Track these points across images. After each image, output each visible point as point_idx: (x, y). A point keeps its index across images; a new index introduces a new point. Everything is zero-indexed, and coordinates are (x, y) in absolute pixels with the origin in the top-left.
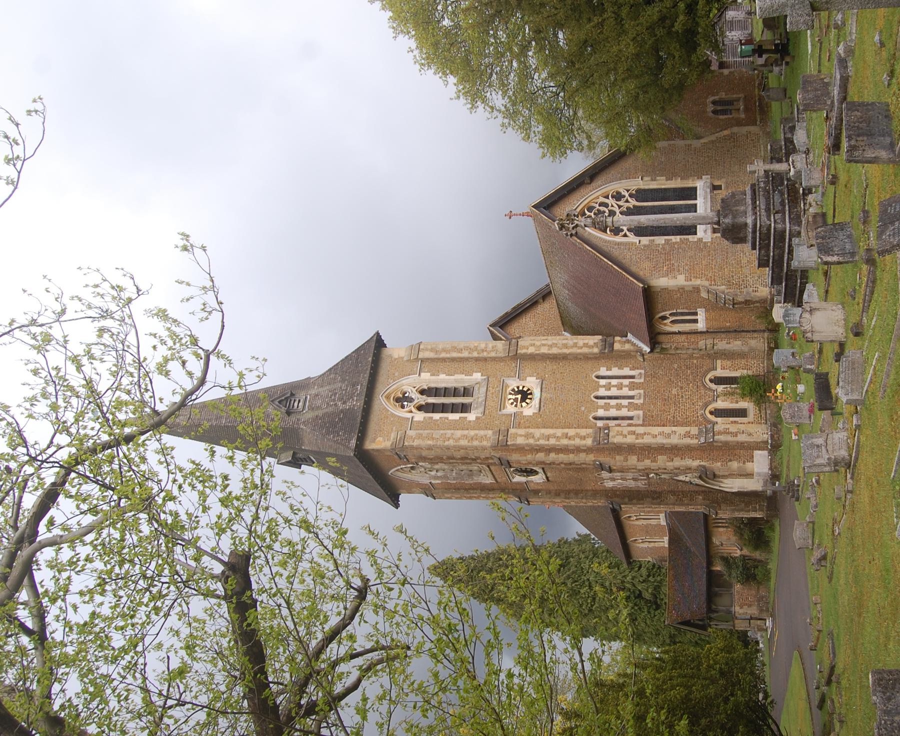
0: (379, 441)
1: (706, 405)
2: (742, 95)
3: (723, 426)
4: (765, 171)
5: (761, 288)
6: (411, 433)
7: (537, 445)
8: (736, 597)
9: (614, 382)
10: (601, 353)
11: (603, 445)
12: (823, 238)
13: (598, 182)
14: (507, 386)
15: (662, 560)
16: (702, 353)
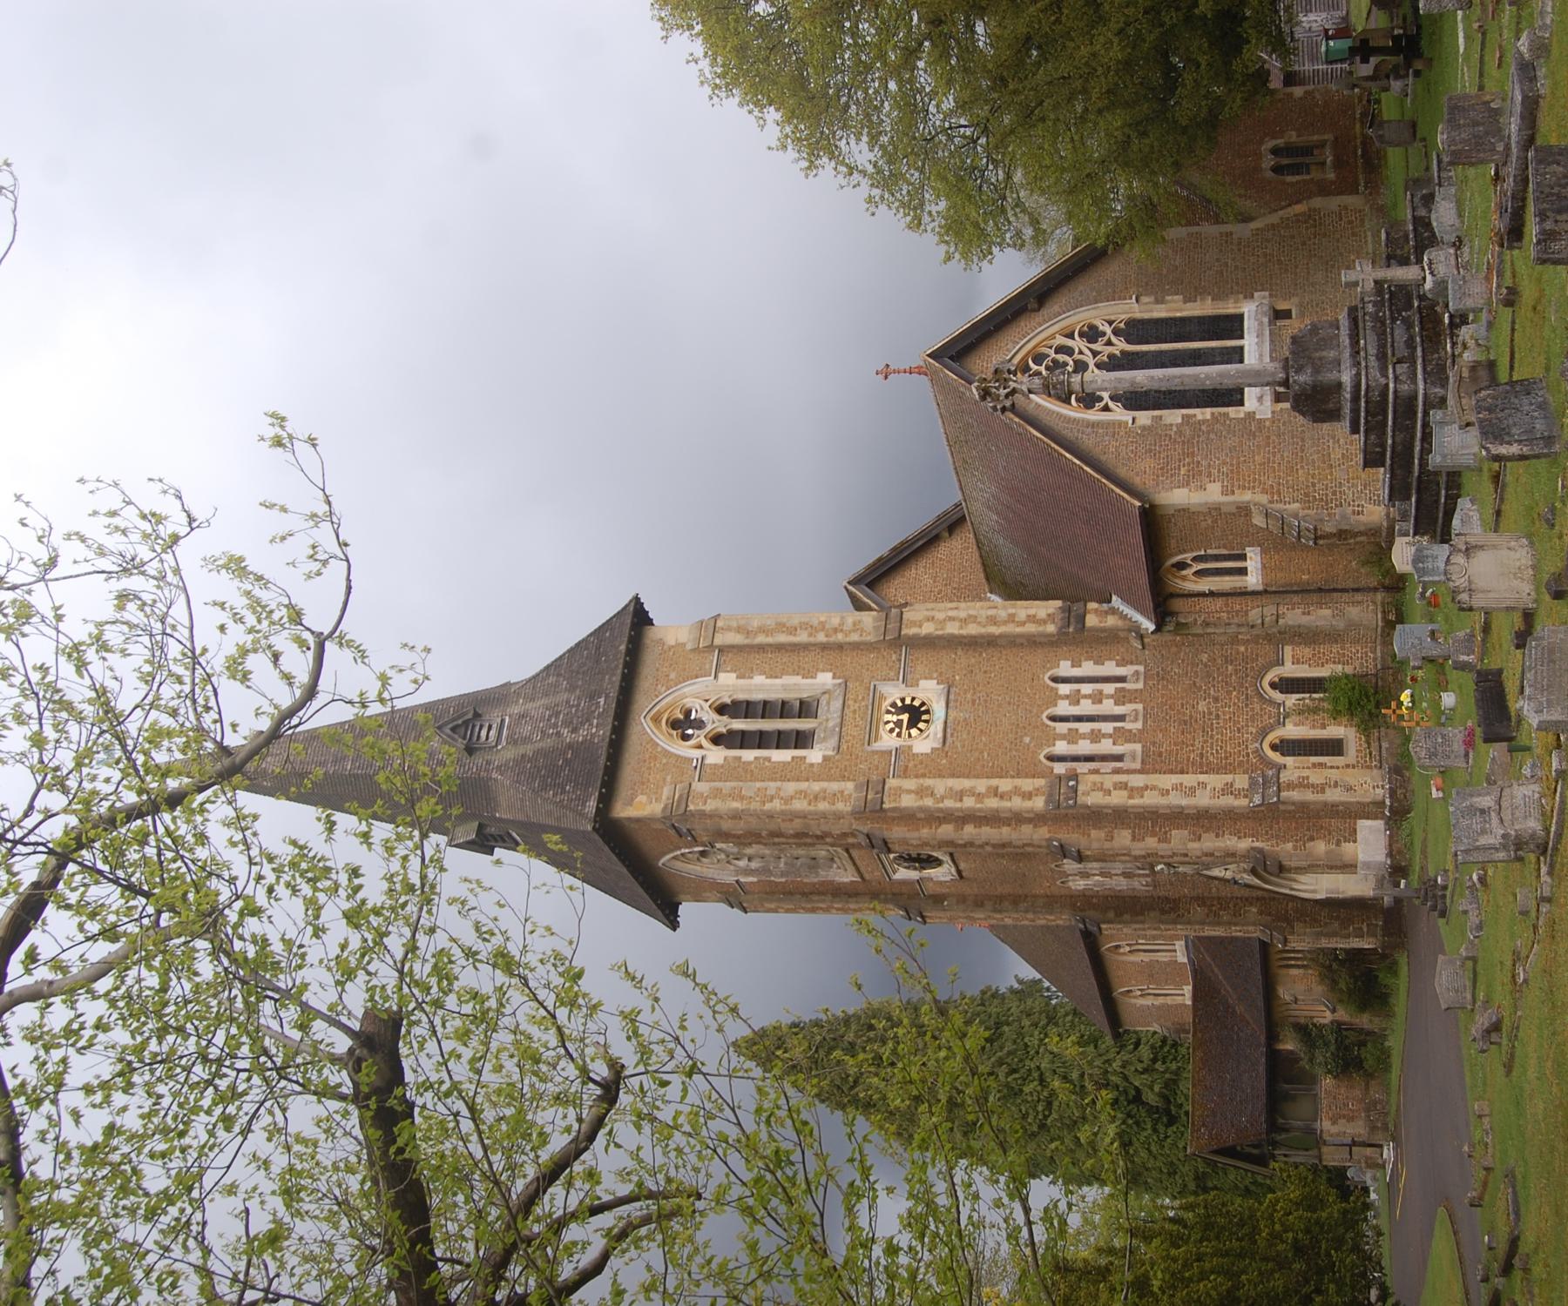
0: (640, 804)
1: (1264, 733)
2: (1328, 137)
4: (1376, 282)
5: (1369, 507)
6: (700, 787)
7: (941, 810)
9: (1087, 689)
10: (1062, 633)
11: (1066, 809)
12: (1490, 410)
13: (1053, 307)
15: (1181, 1029)
16: (1255, 632)
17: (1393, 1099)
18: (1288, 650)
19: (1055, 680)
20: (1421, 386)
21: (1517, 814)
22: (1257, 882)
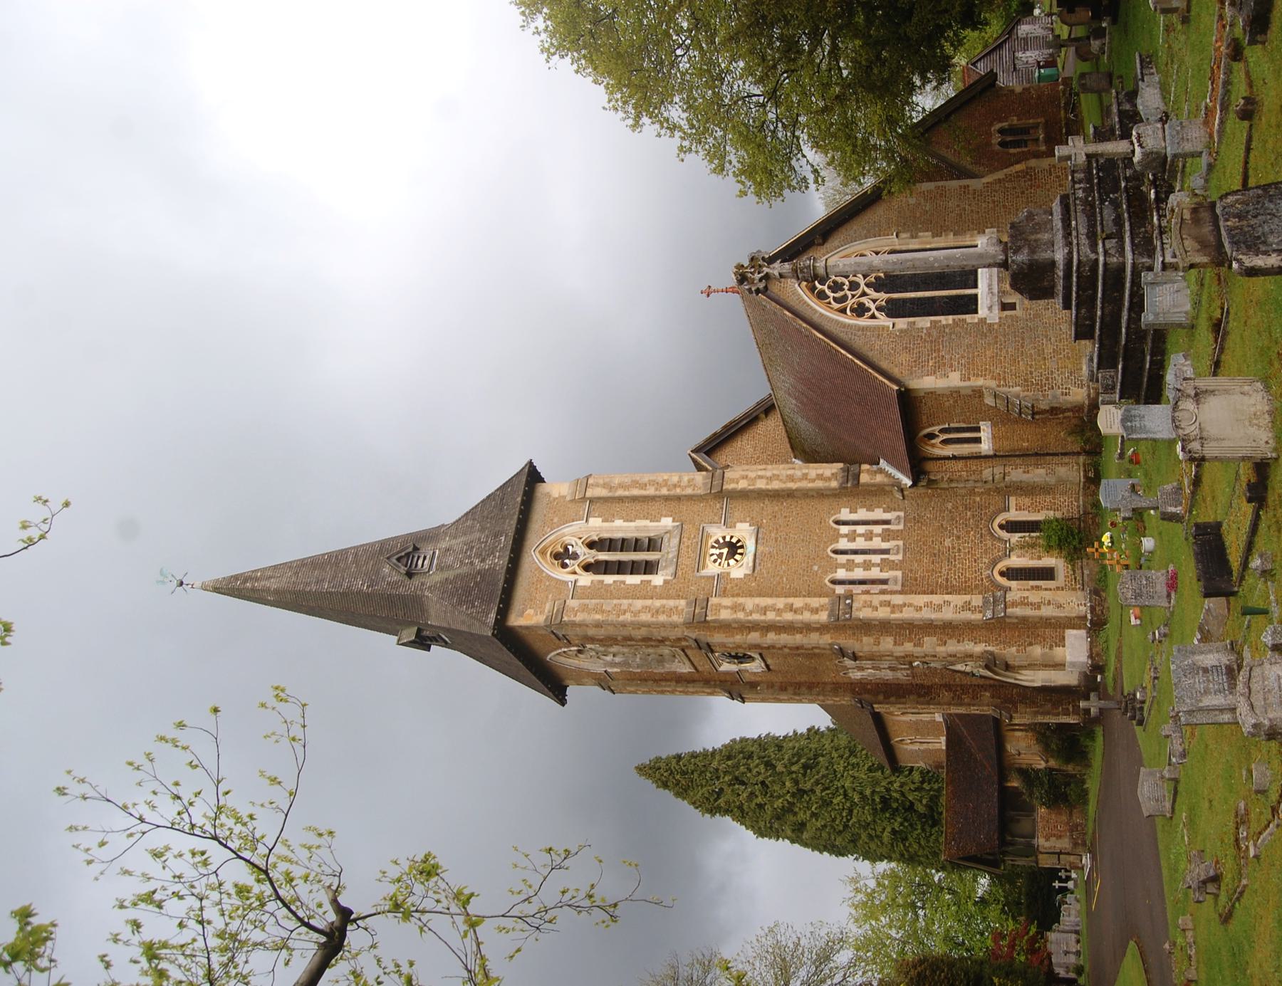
1: (994, 563)
2: (1041, 120)
3: (1020, 594)
4: (1088, 156)
5: (1074, 389)
6: (572, 603)
7: (749, 622)
8: (1040, 825)
9: (861, 529)
10: (842, 488)
11: (843, 622)
12: (1240, 216)
13: (834, 241)
14: (709, 536)
15: (939, 766)
16: (988, 486)
17: (1090, 825)
18: (1013, 500)
19: (838, 522)
20: (1129, 256)
21: (1271, 699)
22: (989, 674)
